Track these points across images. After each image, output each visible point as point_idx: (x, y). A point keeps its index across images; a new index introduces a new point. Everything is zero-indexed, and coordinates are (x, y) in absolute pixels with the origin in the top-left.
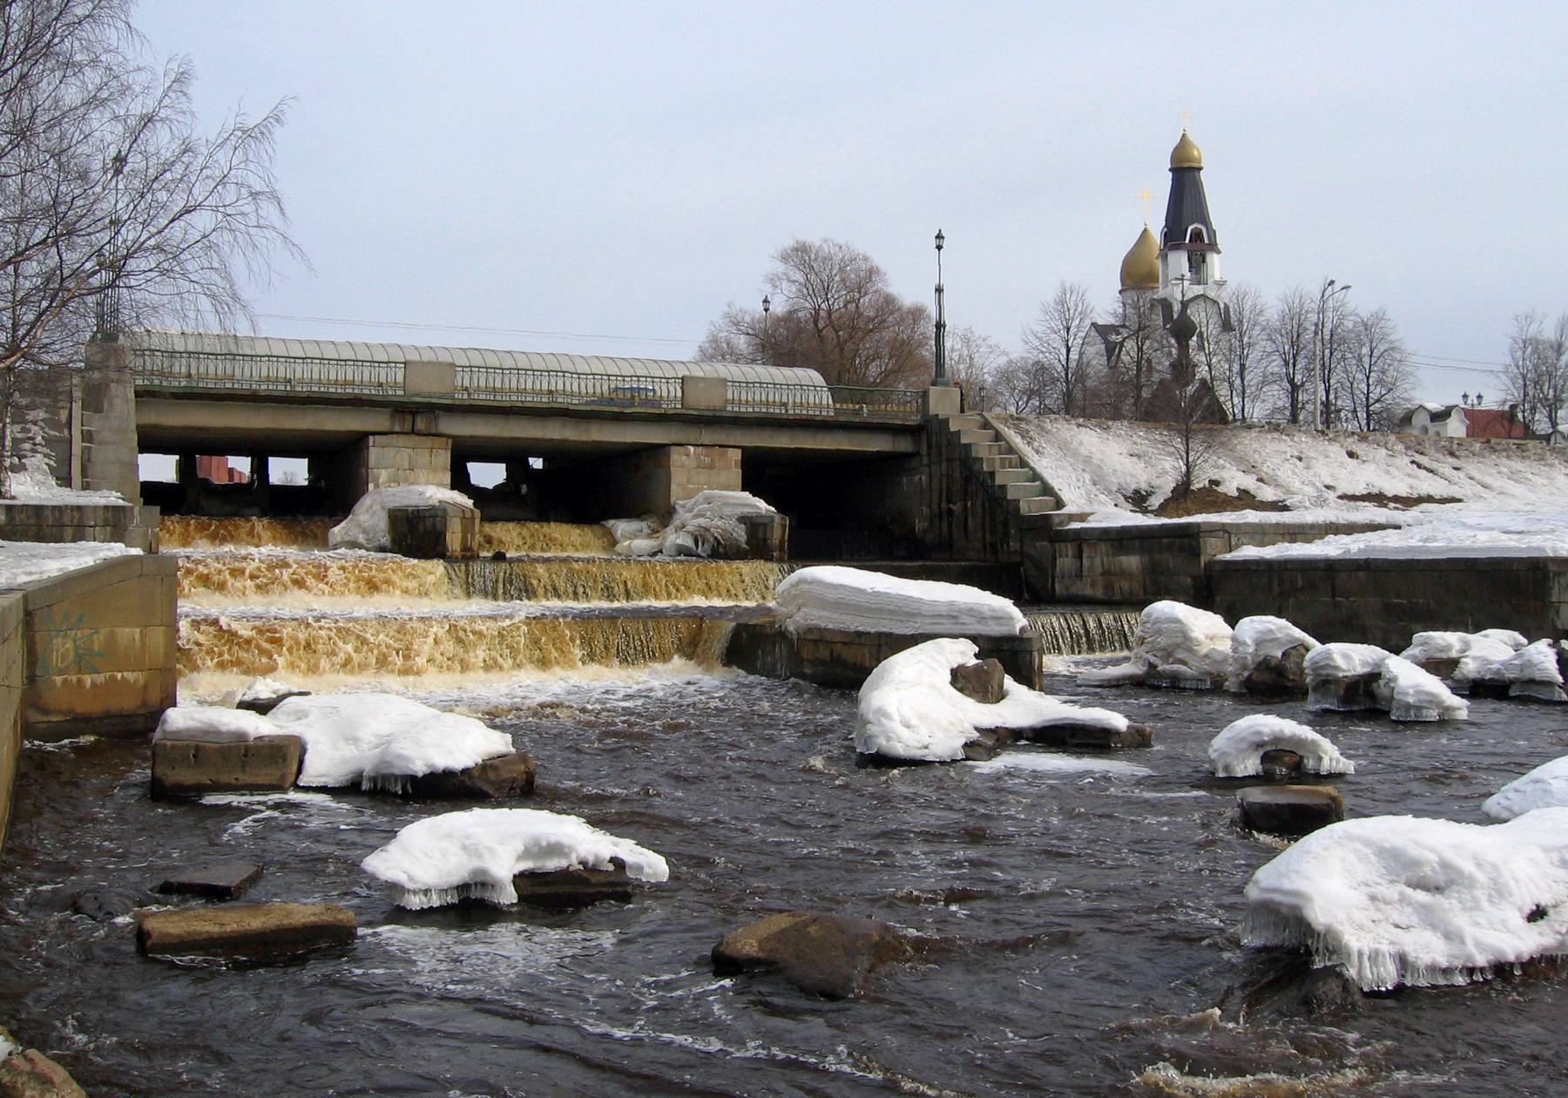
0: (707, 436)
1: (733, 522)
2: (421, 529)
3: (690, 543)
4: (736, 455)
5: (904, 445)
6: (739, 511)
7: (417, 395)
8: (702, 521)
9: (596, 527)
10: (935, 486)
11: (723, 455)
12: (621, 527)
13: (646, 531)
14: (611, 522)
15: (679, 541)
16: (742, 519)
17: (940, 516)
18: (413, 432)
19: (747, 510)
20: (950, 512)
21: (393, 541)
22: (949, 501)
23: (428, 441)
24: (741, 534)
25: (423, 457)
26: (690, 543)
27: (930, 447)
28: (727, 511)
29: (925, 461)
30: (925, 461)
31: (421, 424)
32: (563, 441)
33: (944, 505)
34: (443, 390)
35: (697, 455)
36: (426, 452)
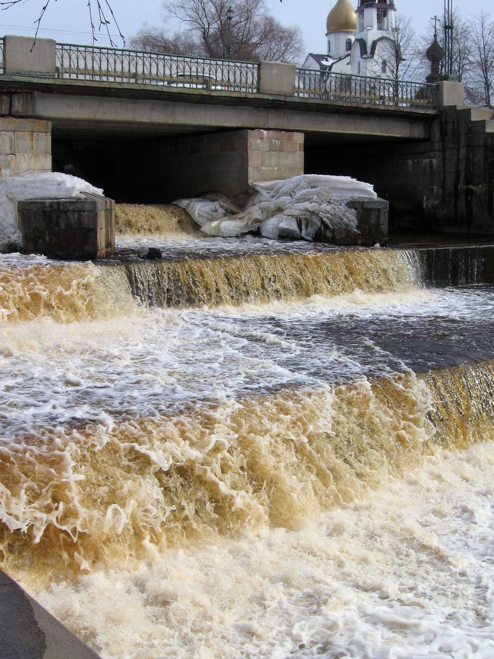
0: (274, 121)
1: (343, 207)
2: (63, 225)
3: (293, 226)
4: (299, 138)
5: (416, 132)
6: (348, 196)
7: (19, 74)
8: (307, 205)
9: (171, 208)
10: (450, 167)
11: (290, 139)
12: (199, 208)
13: (221, 211)
14: (184, 203)
15: (283, 225)
16: (352, 204)
17: (456, 194)
18: (11, 115)
19: (357, 195)
20: (469, 192)
21: (26, 238)
22: (468, 182)
23: (27, 124)
24: (351, 218)
25: (24, 140)
26: (293, 226)
27: (443, 134)
28: (335, 196)
29: (437, 146)
30: (437, 146)
31: (18, 106)
32: (152, 124)
33: (462, 186)
34: (44, 70)
35: (269, 139)
36: (27, 135)
